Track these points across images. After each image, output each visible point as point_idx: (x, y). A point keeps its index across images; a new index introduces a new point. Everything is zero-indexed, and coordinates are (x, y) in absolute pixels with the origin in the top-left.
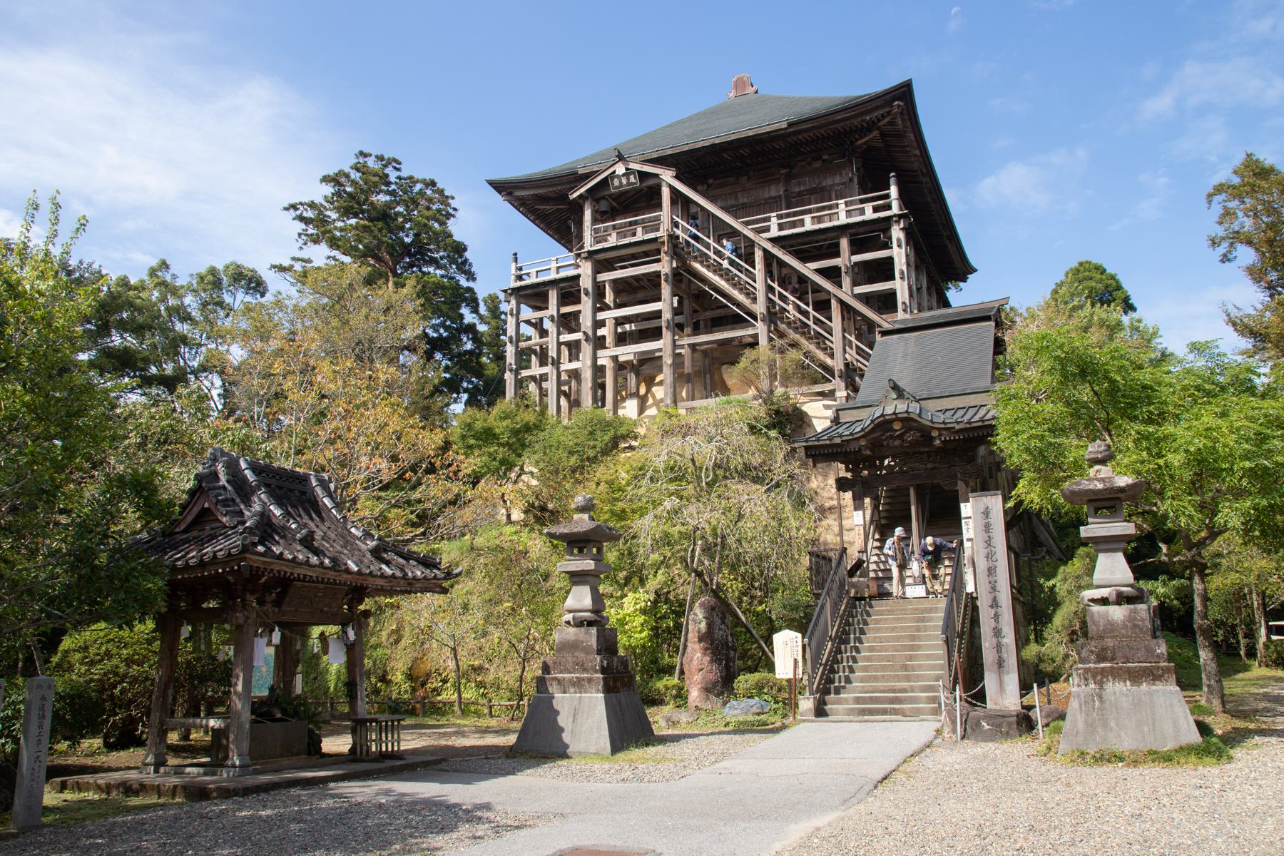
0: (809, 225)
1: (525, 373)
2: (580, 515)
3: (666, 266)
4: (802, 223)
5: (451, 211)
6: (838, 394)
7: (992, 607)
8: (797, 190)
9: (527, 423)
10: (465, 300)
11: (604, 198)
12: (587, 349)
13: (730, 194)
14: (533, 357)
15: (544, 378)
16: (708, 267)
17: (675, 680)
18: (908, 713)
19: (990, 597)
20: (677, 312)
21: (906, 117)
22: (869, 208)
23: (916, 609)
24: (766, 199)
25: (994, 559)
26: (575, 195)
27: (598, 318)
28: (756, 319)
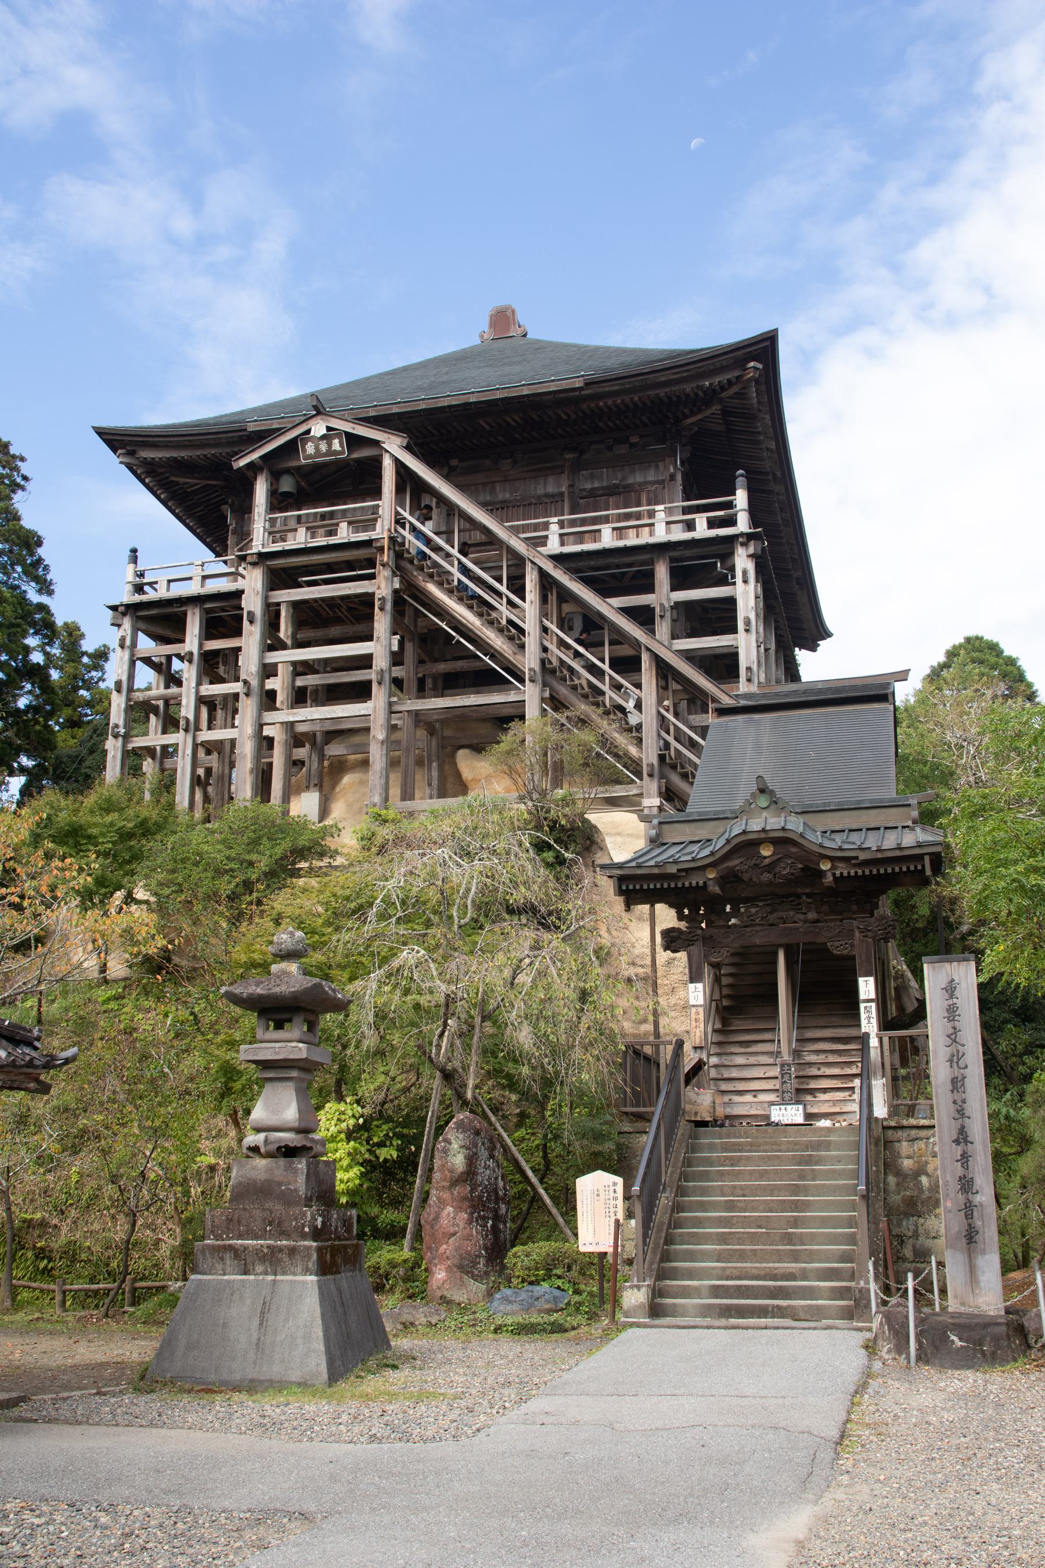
0: (607, 539)
1: (139, 742)
2: (283, 965)
3: (383, 585)
4: (596, 534)
5: (19, 480)
6: (646, 802)
7: (957, 1142)
8: (588, 486)
9: (144, 822)
10: (33, 624)
11: (288, 471)
12: (248, 708)
13: (484, 485)
14: (152, 717)
15: (168, 752)
16: (450, 592)
17: (405, 1253)
18: (802, 1315)
19: (955, 1126)
20: (397, 659)
21: (763, 388)
22: (701, 521)
23: (796, 1143)
24: (539, 497)
25: (961, 1064)
26: (242, 463)
27: (268, 661)
28: (522, 681)
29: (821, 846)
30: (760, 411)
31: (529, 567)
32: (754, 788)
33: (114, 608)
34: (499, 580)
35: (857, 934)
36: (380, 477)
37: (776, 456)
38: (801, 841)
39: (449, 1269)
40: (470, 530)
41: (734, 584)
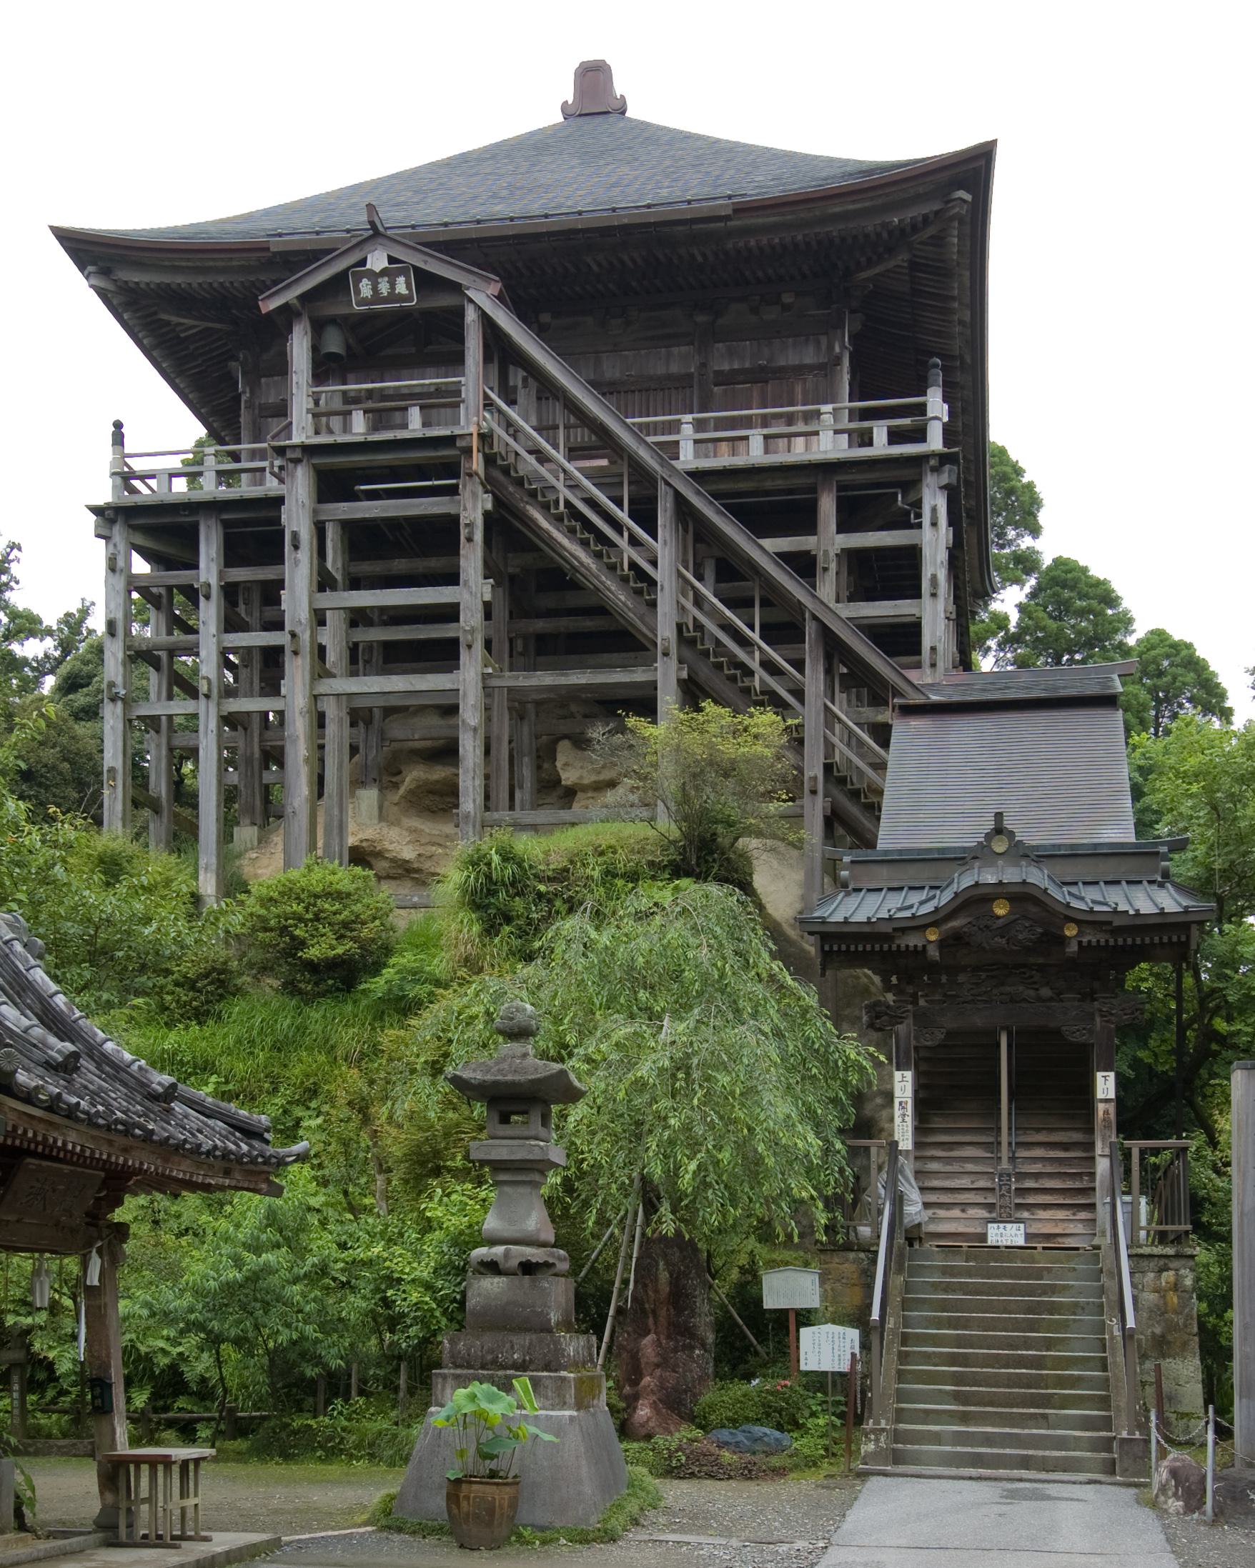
0: (755, 452)
29: (1068, 905)
30: (958, 264)
31: (662, 488)
32: (990, 825)
33: (97, 510)
34: (619, 503)
35: (1098, 1019)
36: (461, 339)
37: (969, 332)
38: (1043, 898)
39: (654, 1406)
40: (576, 427)
41: (919, 526)
